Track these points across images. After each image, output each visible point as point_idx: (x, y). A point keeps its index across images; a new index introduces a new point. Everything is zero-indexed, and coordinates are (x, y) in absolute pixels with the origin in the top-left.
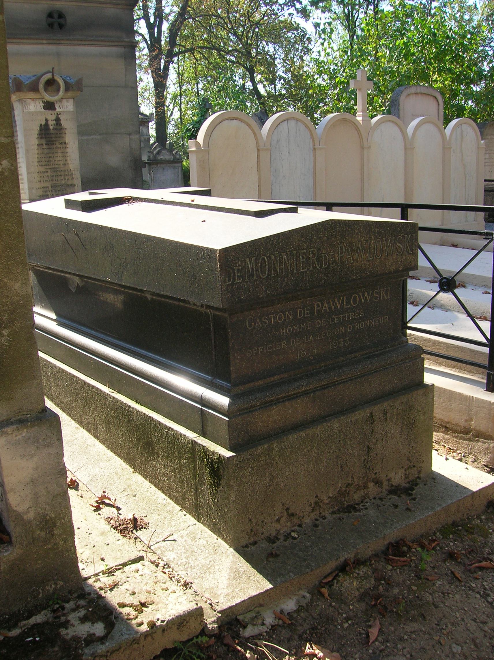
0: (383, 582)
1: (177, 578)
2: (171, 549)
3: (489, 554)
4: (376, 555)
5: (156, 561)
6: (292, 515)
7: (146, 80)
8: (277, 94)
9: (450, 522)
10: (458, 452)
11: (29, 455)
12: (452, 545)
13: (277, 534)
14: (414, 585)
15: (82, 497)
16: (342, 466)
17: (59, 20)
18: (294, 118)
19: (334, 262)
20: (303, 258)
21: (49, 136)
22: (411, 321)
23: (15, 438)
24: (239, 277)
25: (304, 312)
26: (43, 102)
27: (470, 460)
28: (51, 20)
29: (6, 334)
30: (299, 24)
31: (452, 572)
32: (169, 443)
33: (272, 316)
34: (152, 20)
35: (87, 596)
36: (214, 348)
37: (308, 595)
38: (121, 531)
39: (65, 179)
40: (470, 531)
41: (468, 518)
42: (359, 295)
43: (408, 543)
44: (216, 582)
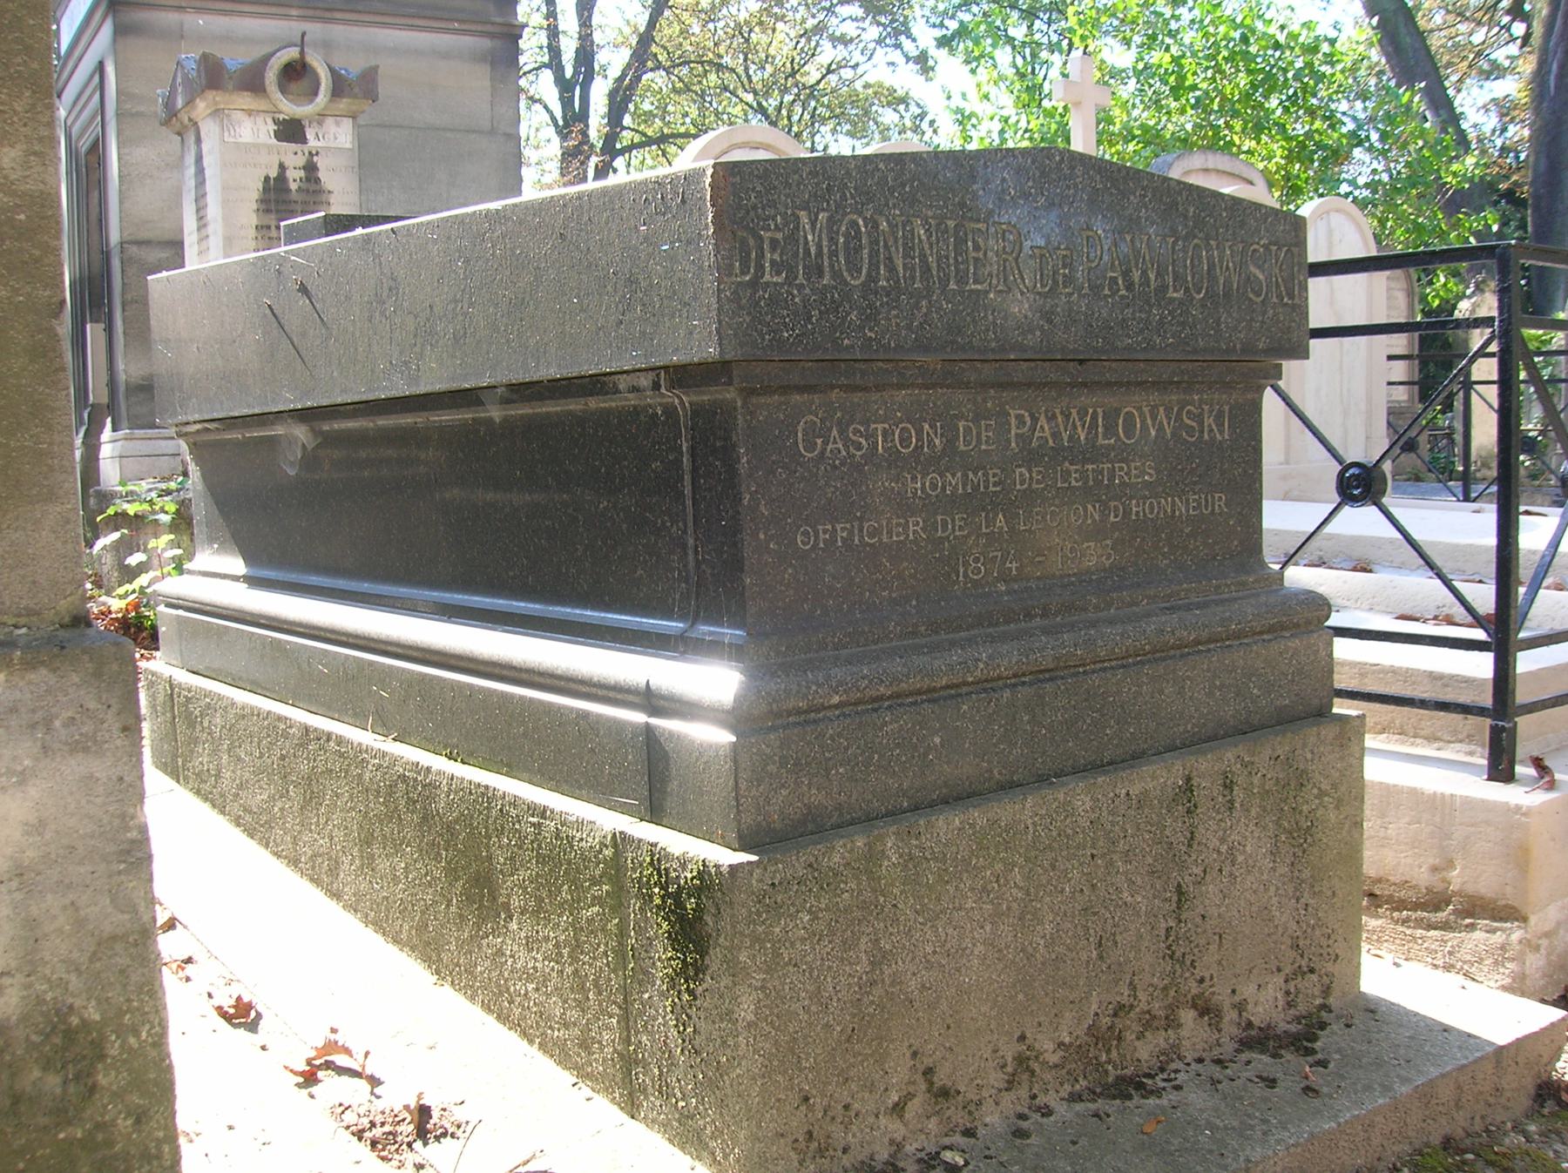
6: (945, 1093)
9: (1436, 1139)
16: (1100, 945)
32: (542, 860)
33: (880, 426)
34: (569, 73)
36: (690, 524)
41: (1487, 1131)
42: (1139, 409)
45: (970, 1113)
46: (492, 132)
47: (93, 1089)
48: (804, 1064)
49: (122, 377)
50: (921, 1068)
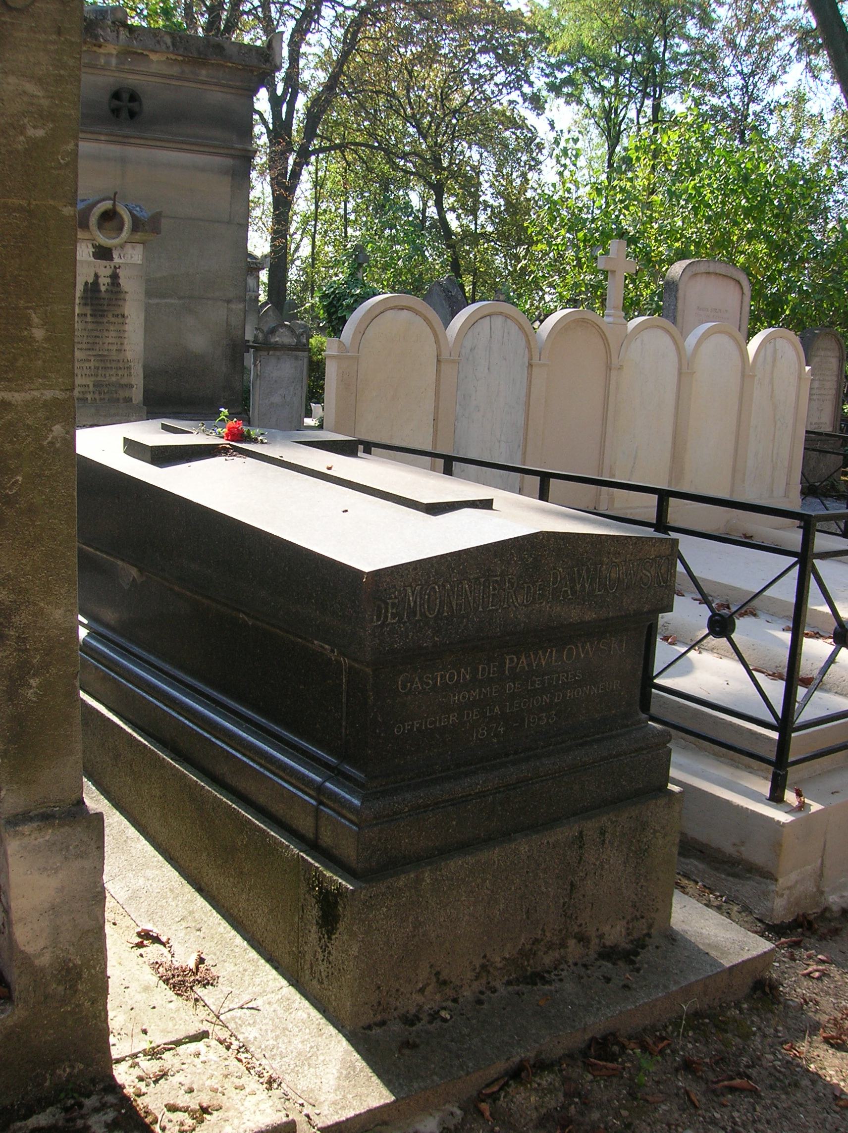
0: (577, 1100)
1: (259, 1069)
2: (251, 1022)
3: (748, 1067)
4: (570, 1056)
5: (228, 1040)
6: (445, 983)
7: (261, 189)
11: (52, 869)
13: (418, 1011)
14: (626, 1109)
18: (501, 314)
20: (494, 589)
24: (394, 616)
25: (489, 670)
26: (94, 246)
28: (117, 102)
29: (34, 685)
31: (687, 1093)
34: (279, 91)
37: (459, 1112)
38: (174, 987)
40: (722, 1027)
41: (721, 1006)
43: (621, 1039)
44: (318, 1081)
46: (229, 222)
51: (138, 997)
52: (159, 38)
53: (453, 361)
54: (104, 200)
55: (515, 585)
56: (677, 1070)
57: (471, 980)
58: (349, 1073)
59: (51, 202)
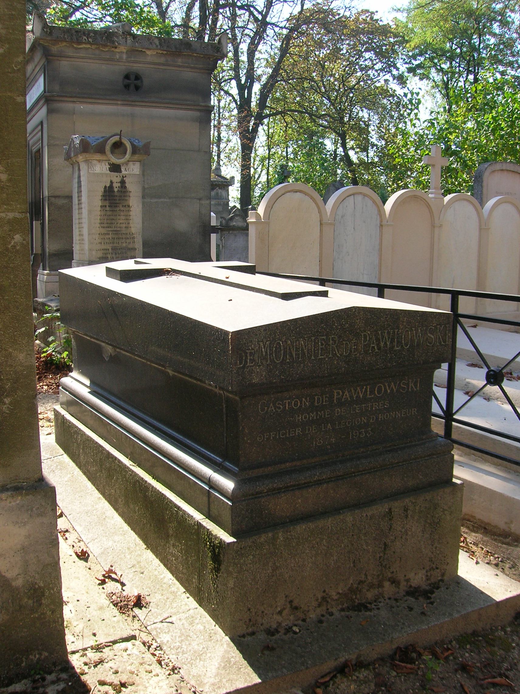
0: (383, 688)
2: (167, 631)
3: (507, 670)
4: (382, 659)
5: (150, 642)
6: (296, 608)
8: (369, 161)
9: (470, 631)
10: (496, 556)
12: (467, 656)
13: (277, 627)
15: (90, 569)
16: (354, 562)
17: (136, 82)
18: (361, 193)
19: (356, 350)
20: (322, 344)
21: (114, 198)
22: (458, 413)
23: (9, 505)
25: (323, 400)
27: (507, 566)
28: (128, 81)
29: (7, 402)
30: (395, 91)
31: (462, 686)
33: (287, 401)
35: (70, 670)
36: (225, 430)
38: (121, 608)
39: (126, 242)
40: (490, 643)
41: (491, 629)
43: (418, 649)
44: (205, 670)
45: (305, 614)
46: (199, 151)
47: (41, 604)
48: (249, 599)
49: (47, 250)
50: (288, 600)
51: (95, 613)
52: (151, 41)
53: (330, 224)
54: (114, 135)
55: (337, 342)
56: (456, 671)
57: (315, 607)
58: (226, 665)
59: (9, 94)
